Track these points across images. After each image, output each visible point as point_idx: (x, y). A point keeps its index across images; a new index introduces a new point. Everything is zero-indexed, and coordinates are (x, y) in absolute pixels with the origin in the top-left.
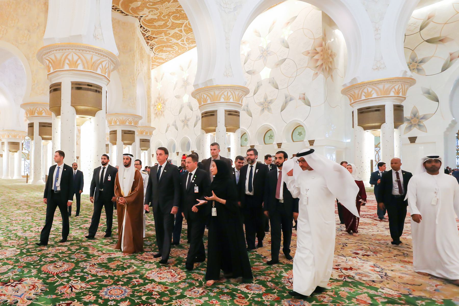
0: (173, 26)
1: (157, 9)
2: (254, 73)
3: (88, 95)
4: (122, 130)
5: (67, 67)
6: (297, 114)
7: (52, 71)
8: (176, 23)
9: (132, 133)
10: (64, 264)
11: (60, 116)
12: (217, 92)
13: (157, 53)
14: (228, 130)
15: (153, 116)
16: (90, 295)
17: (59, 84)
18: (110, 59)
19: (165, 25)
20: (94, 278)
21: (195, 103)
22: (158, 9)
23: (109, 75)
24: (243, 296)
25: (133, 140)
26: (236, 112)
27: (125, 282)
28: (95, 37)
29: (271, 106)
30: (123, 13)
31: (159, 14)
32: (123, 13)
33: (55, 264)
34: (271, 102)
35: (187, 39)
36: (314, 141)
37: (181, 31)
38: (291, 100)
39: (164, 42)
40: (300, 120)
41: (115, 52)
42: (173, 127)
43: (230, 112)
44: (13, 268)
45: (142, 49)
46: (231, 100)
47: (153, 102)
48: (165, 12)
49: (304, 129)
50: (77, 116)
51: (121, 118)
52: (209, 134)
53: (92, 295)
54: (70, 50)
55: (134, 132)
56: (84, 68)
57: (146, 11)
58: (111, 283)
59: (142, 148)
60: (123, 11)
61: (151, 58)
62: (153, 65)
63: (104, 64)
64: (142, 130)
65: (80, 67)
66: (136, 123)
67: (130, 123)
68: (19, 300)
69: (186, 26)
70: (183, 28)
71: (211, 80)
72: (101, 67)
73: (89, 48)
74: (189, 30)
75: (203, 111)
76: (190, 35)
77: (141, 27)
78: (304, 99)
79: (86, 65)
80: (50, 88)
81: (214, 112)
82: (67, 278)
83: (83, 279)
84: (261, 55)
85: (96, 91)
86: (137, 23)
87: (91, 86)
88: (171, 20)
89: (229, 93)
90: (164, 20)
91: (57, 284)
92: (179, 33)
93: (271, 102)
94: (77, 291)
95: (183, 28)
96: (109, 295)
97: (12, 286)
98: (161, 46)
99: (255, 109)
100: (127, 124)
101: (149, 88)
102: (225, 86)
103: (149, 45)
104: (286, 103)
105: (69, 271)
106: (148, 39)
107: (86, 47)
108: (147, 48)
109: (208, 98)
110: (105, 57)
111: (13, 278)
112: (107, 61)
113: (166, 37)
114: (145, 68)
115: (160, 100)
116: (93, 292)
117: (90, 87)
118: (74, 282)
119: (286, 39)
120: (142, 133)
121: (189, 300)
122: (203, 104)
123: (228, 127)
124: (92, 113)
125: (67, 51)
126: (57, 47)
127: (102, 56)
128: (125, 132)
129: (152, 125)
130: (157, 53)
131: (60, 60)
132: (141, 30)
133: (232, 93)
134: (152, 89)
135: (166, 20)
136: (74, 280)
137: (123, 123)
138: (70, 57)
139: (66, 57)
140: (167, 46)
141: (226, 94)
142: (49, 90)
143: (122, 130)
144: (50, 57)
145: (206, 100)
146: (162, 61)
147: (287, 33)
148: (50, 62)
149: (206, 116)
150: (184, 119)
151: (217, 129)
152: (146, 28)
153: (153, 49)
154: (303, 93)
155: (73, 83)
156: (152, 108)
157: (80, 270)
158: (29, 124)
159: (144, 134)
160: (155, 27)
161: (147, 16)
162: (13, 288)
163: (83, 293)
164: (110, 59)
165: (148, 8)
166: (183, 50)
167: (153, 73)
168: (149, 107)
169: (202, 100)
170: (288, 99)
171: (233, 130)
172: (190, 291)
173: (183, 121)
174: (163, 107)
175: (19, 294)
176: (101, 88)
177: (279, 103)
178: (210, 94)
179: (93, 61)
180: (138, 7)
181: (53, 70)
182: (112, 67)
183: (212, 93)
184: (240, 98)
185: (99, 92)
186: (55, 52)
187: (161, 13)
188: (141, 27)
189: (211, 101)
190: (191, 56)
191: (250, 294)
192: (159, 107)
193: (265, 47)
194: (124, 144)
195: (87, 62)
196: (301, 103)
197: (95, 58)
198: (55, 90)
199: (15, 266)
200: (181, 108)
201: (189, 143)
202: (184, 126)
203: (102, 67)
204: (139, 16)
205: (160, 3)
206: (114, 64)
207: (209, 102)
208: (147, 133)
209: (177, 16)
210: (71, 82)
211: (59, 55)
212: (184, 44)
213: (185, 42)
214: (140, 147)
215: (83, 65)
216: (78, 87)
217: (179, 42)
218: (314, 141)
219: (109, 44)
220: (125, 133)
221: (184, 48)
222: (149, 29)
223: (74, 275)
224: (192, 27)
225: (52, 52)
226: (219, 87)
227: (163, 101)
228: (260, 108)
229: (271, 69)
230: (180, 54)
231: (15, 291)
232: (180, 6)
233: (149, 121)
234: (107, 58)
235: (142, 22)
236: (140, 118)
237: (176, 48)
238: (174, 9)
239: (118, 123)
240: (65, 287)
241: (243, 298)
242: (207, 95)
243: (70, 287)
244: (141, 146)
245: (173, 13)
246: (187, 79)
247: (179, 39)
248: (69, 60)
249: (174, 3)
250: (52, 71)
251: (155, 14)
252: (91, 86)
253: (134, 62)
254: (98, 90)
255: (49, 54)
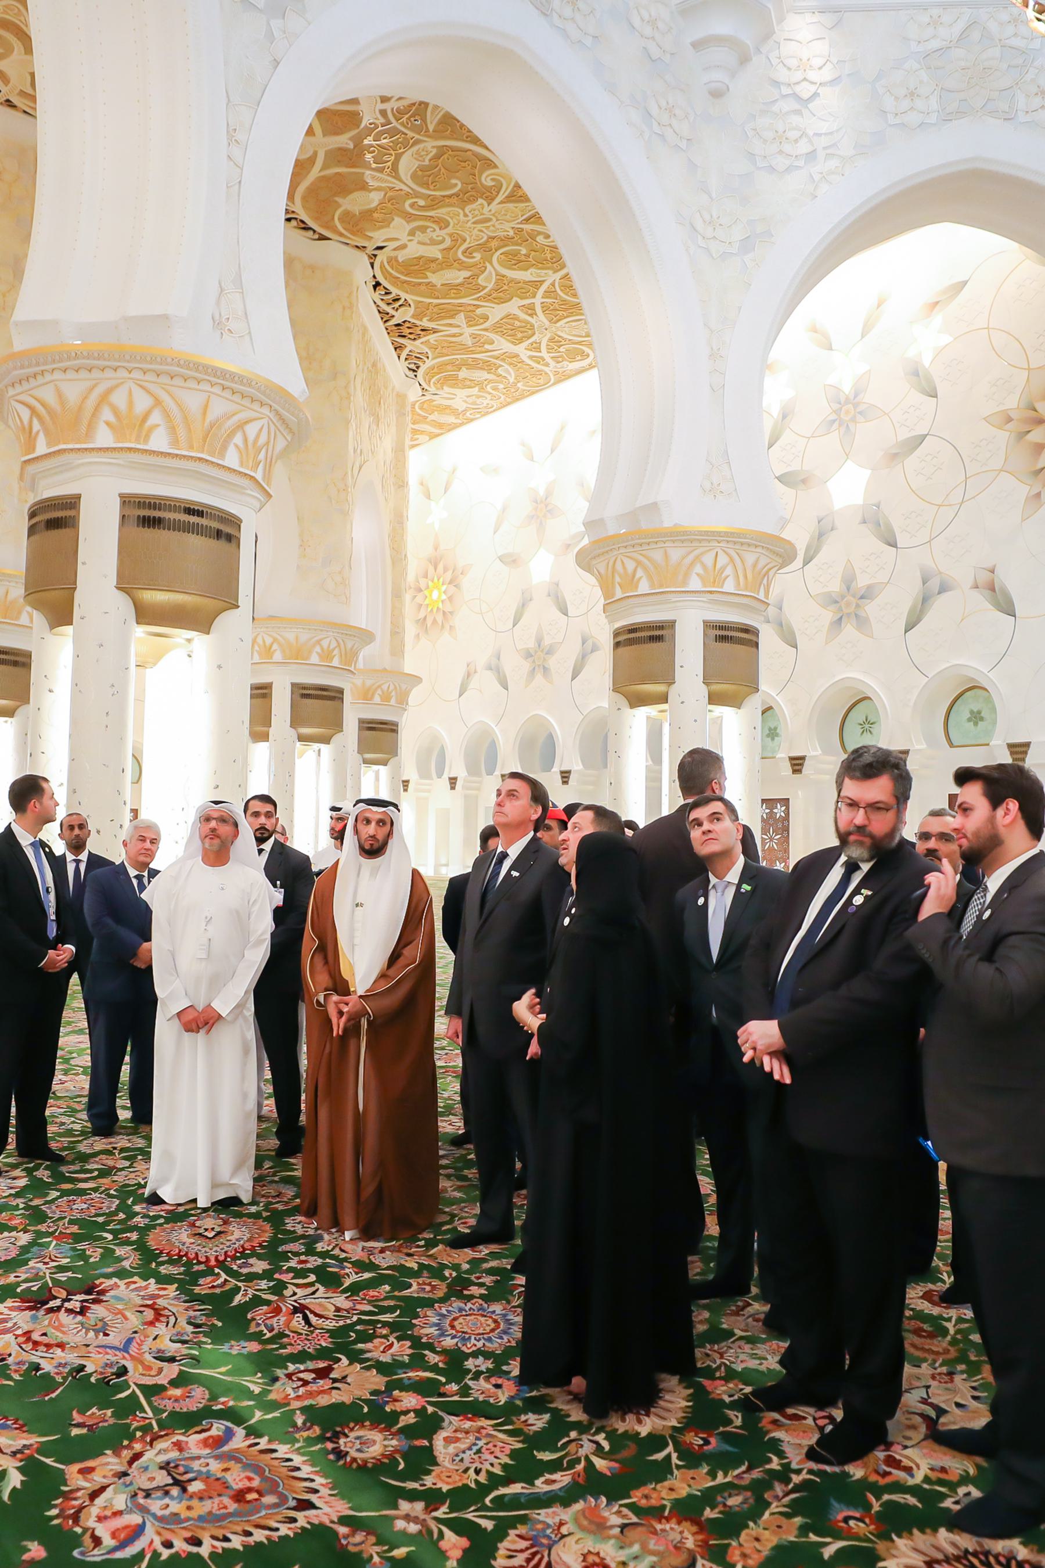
0: (502, 292)
1: (442, 223)
2: (804, 481)
3: (182, 550)
4: (293, 685)
5: (104, 437)
6: (964, 641)
7: (42, 447)
8: (512, 280)
9: (332, 695)
10: (226, 1222)
11: (68, 630)
12: (676, 554)
13: (432, 389)
14: (714, 699)
15: (410, 630)
16: (385, 1337)
17: (72, 503)
18: (277, 413)
19: (471, 285)
20: (367, 1275)
21: (585, 591)
22: (447, 225)
23: (268, 474)
24: (926, 1327)
25: (337, 724)
26: (746, 630)
27: (488, 1288)
28: (218, 324)
29: (871, 609)
30: (307, 228)
31: (448, 242)
32: (307, 228)
33: (193, 1225)
34: (868, 594)
35: (551, 340)
36: (1027, 745)
37: (530, 310)
38: (943, 589)
39: (465, 349)
40: (976, 664)
41: (292, 379)
42: (490, 676)
43: (721, 628)
44: (33, 1243)
45: (375, 368)
46: (729, 586)
47: (411, 577)
48: (474, 235)
49: (989, 700)
50: (140, 631)
51: (290, 636)
52: (643, 714)
53: (392, 1339)
54: (122, 373)
55: (341, 691)
56: (175, 442)
57: (399, 229)
58: (440, 1294)
59: (368, 756)
60: (311, 223)
61: (409, 408)
62: (415, 431)
63: (252, 430)
64: (369, 683)
65: (159, 441)
66: (350, 657)
67: (327, 655)
68: (129, 1365)
69: (548, 293)
70: (538, 301)
71: (654, 507)
72: (241, 444)
73: (197, 367)
74: (566, 305)
75: (618, 625)
76: (565, 329)
77: (377, 285)
78: (993, 590)
79: (181, 432)
80: (32, 515)
81: (661, 628)
82: (267, 1275)
83: (330, 1280)
84: (834, 417)
85: (219, 534)
86: (362, 272)
87: (200, 514)
88: (495, 268)
89: (723, 560)
90: (467, 268)
91: (238, 1299)
92: (523, 316)
93: (868, 594)
94: (331, 1325)
95: (538, 301)
96: (454, 1337)
97: (70, 1311)
98: (451, 363)
99: (808, 616)
100: (315, 659)
101: (399, 520)
102: (706, 533)
103: (403, 356)
104: (925, 600)
105: (259, 1250)
106: (400, 332)
107: (187, 364)
108: (395, 368)
109: (640, 573)
110: (256, 406)
111: (57, 1283)
112: (265, 421)
113: (472, 330)
114: (387, 444)
115: (440, 567)
116: (393, 1326)
117: (193, 519)
118: (300, 1292)
119: (927, 364)
120: (366, 695)
121: (747, 1348)
122: (619, 594)
123: (716, 687)
124: (200, 621)
125: (109, 373)
126: (69, 359)
127: (246, 402)
128: (303, 693)
129: (409, 667)
130: (432, 389)
131: (80, 408)
132: (377, 296)
133: (732, 560)
134: (412, 527)
135: (475, 265)
136: (297, 1286)
137: (297, 654)
138: (119, 399)
139: (104, 398)
140: (475, 365)
141: (708, 559)
142: (25, 525)
143: (293, 685)
144: (40, 393)
145: (631, 581)
146: (452, 419)
147: (929, 342)
148: (33, 410)
149: (631, 642)
150: (531, 644)
151: (673, 692)
152: (395, 291)
153: (420, 373)
154: (989, 565)
155: (127, 501)
156: (408, 597)
157: (297, 1247)
158: (616, 634)
159: (377, 699)
160: (431, 290)
161: (403, 247)
162: (79, 1318)
163: (355, 1332)
164: (277, 413)
165: (409, 217)
166: (534, 382)
167: (418, 461)
168: (397, 594)
169: (617, 579)
170: (934, 584)
171: (733, 701)
172: (737, 1313)
173: (528, 655)
174: (450, 598)
175: (115, 1338)
176: (235, 522)
177: (899, 599)
178: (650, 559)
179: (211, 417)
180: (371, 212)
181: (49, 444)
182: (281, 444)
183: (657, 555)
184: (763, 578)
185: (229, 538)
186: (58, 375)
187: (457, 240)
188: (377, 285)
189: (652, 586)
190: (573, 404)
191: (949, 1320)
192: (435, 595)
193: (847, 388)
194: (301, 738)
195: (185, 418)
196: (980, 601)
197: (219, 407)
198: (54, 524)
199: (39, 1234)
200: (524, 605)
201: (550, 742)
202: (532, 672)
203: (246, 440)
204: (371, 246)
205: (454, 200)
206: (291, 431)
207: (644, 587)
208: (386, 698)
209: (518, 252)
210: (121, 496)
211: (73, 391)
212: (539, 360)
213: (544, 353)
214: (360, 751)
215: (172, 430)
216: (146, 515)
217: (522, 350)
218: (1027, 745)
219: (269, 351)
220: (305, 696)
221: (540, 372)
222: (409, 297)
223: (286, 1265)
224: (583, 298)
225: (48, 377)
226: (685, 533)
227: (449, 575)
228: (828, 616)
229: (866, 473)
230: (522, 397)
231: (97, 1332)
232: (535, 218)
233: (397, 650)
234: (266, 410)
235: (382, 266)
236: (366, 636)
237: (506, 370)
238: (507, 229)
239: (278, 656)
240: (277, 1311)
241: (931, 1336)
242: (639, 563)
243: (296, 1310)
244: (363, 747)
245: (506, 240)
246: (549, 493)
247: (521, 341)
248: (116, 412)
249: (511, 205)
250: (42, 447)
251: (433, 242)
252: (200, 514)
253: (348, 422)
254: (224, 531)
255: (33, 383)
